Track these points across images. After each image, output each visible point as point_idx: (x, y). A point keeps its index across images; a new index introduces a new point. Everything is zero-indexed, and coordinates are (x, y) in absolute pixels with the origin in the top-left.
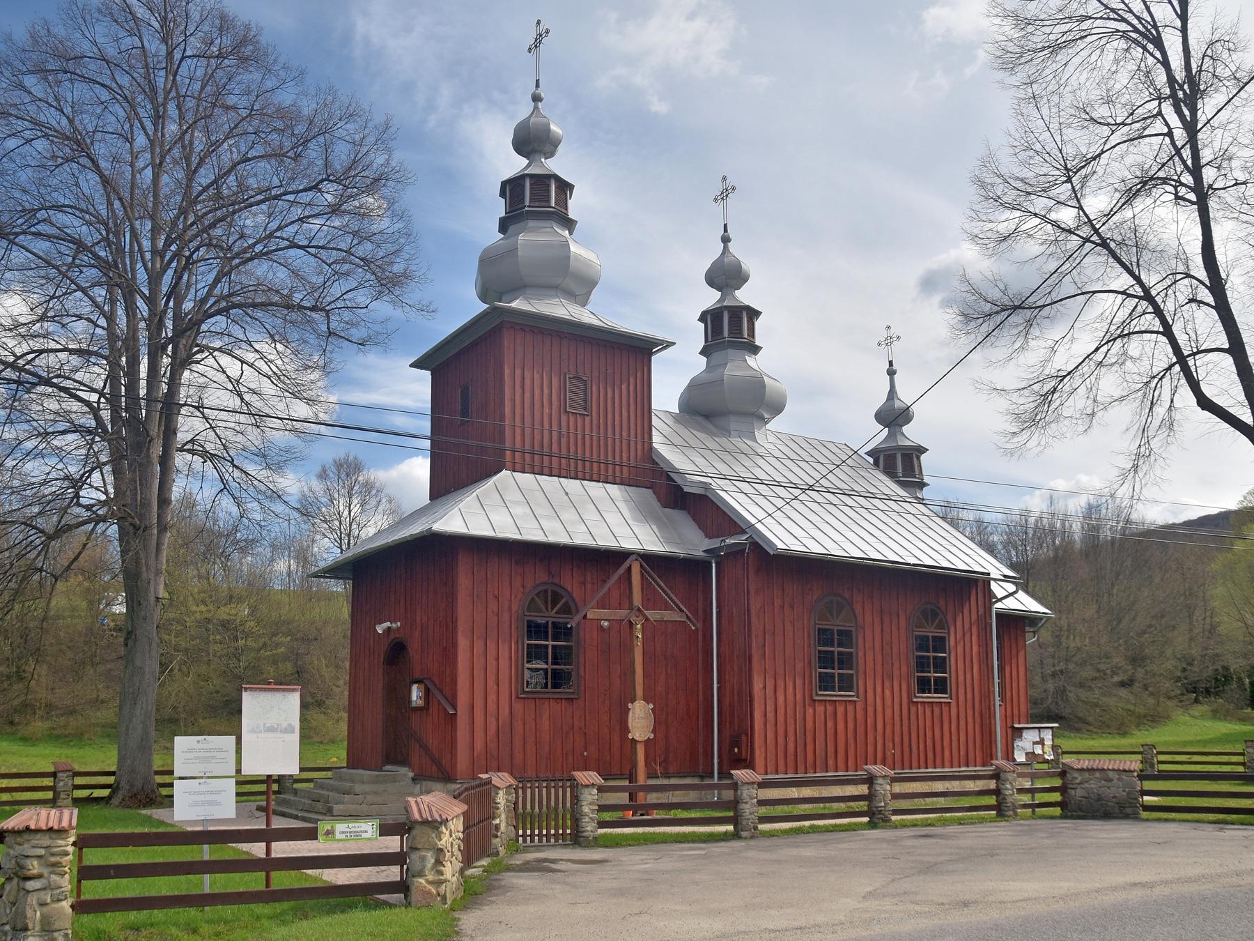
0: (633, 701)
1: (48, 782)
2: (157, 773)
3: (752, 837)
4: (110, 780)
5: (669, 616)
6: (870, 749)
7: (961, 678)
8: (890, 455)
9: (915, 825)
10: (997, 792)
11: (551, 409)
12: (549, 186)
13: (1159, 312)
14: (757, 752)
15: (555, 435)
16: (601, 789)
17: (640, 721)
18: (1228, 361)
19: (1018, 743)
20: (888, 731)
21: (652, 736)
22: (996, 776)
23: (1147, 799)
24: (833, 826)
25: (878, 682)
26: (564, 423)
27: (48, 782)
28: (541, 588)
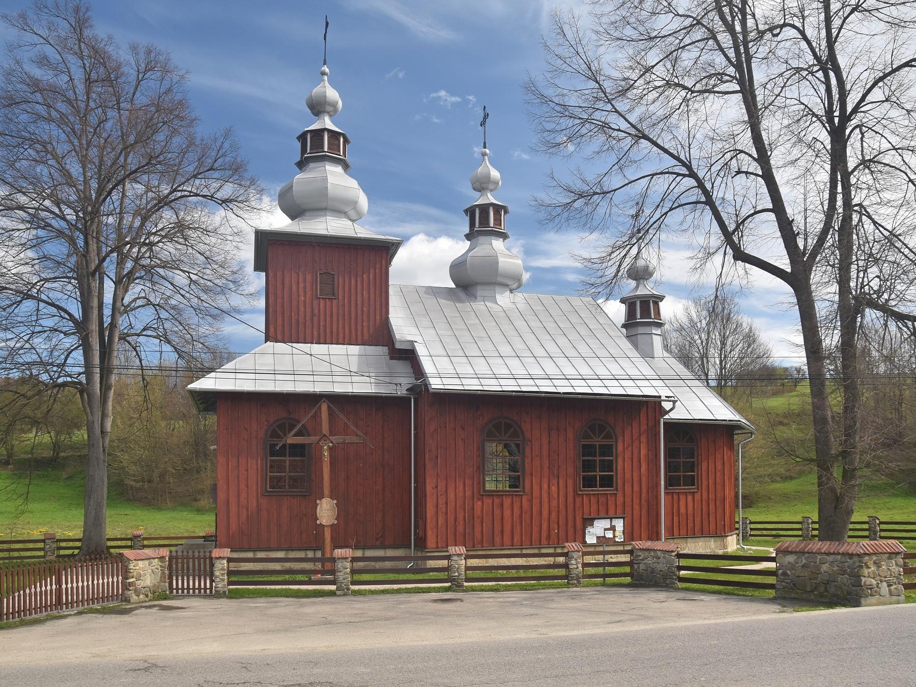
1: (41, 545)
2: (109, 540)
3: (345, 595)
4: (78, 544)
5: (355, 439)
7: (628, 476)
8: (645, 301)
10: (566, 566)
11: (305, 297)
12: (323, 137)
14: (429, 533)
16: (230, 560)
17: (326, 511)
18: (772, 216)
19: (589, 529)
20: (554, 515)
21: (336, 522)
25: (545, 480)
27: (41, 545)
28: (280, 422)
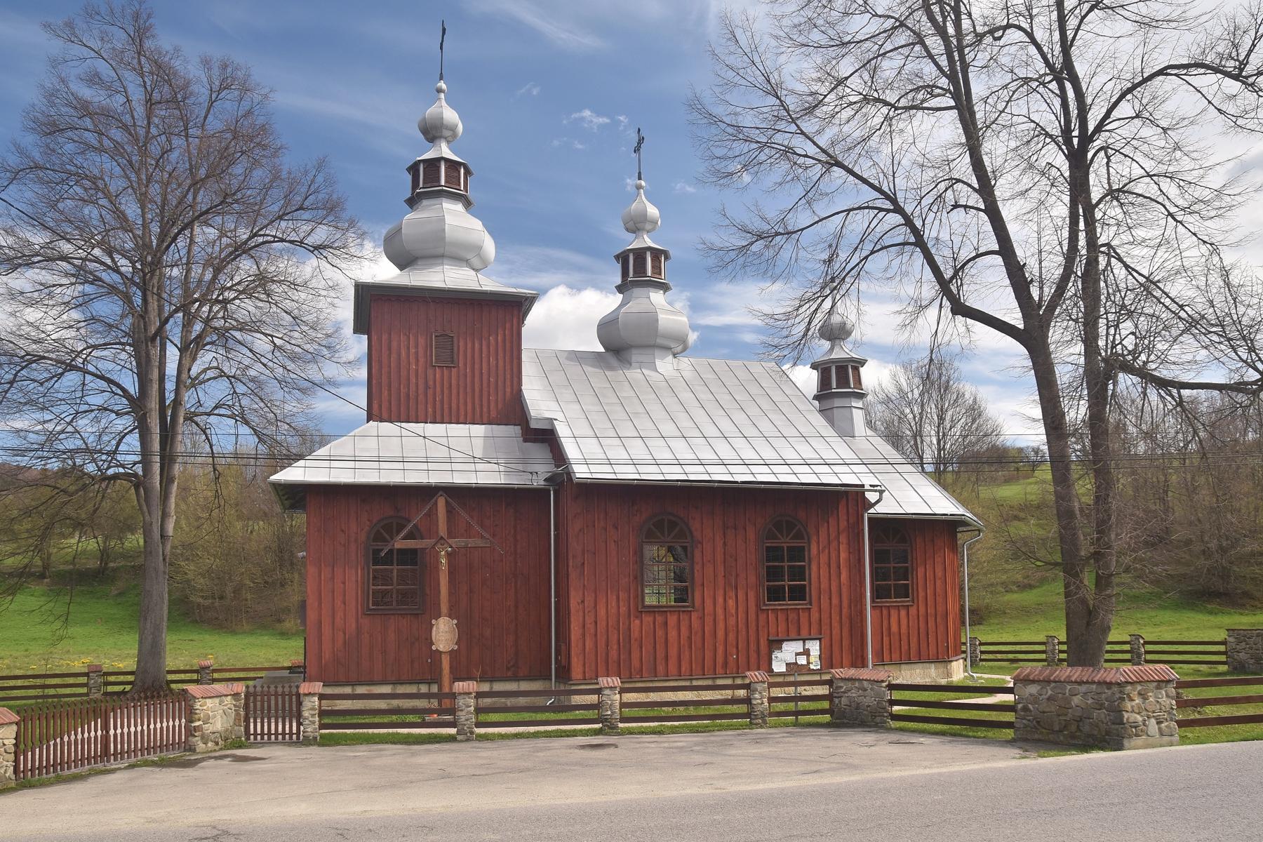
0: (438, 616)
1: (83, 680)
2: (170, 672)
3: (468, 740)
4: (130, 678)
6: (708, 655)
9: (642, 733)
10: (747, 701)
12: (439, 168)
13: (909, 222)
14: (574, 660)
15: (421, 387)
16: (322, 697)
17: (444, 634)
18: (998, 260)
22: (747, 687)
23: (896, 708)
24: (557, 731)
26: (430, 377)
27: (83, 680)
